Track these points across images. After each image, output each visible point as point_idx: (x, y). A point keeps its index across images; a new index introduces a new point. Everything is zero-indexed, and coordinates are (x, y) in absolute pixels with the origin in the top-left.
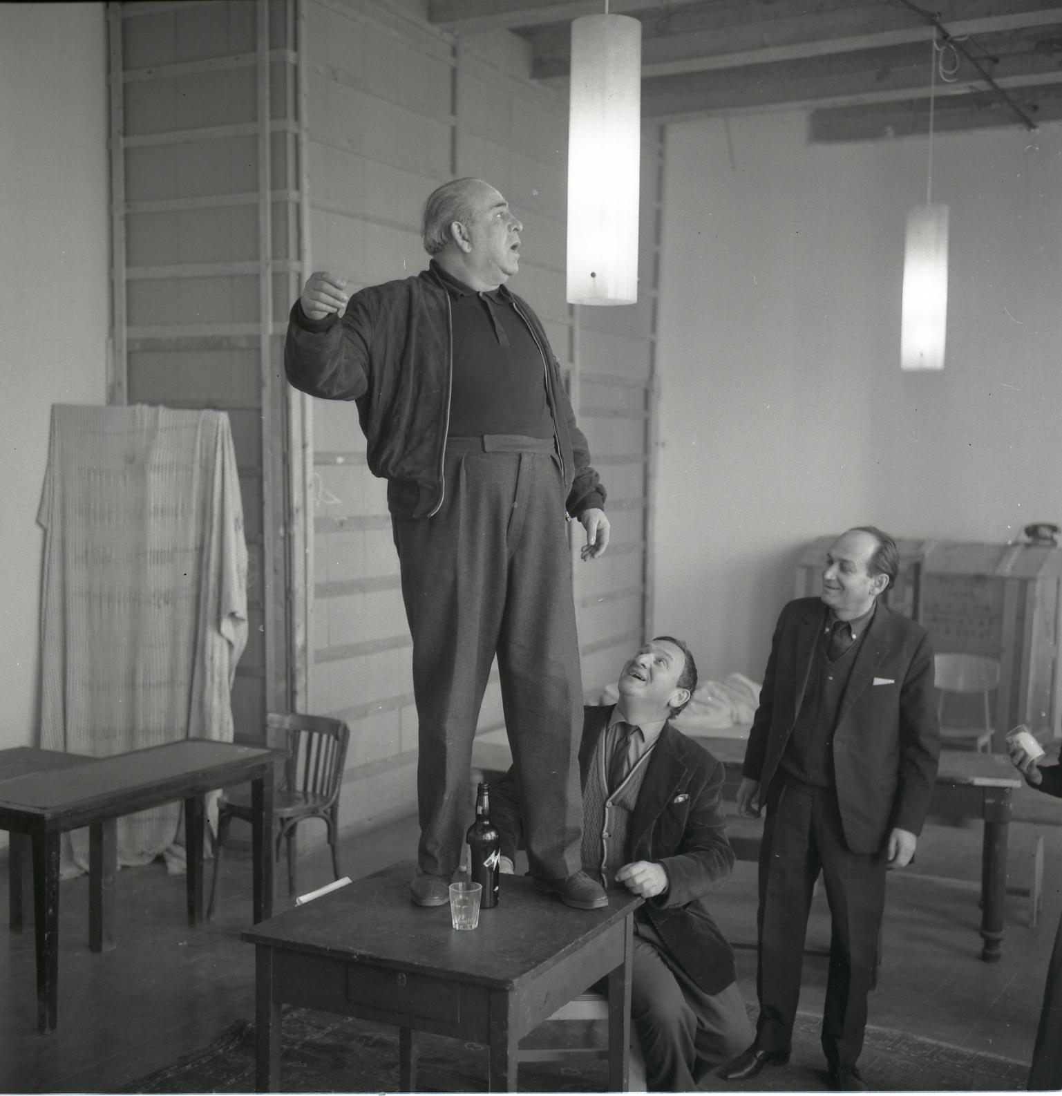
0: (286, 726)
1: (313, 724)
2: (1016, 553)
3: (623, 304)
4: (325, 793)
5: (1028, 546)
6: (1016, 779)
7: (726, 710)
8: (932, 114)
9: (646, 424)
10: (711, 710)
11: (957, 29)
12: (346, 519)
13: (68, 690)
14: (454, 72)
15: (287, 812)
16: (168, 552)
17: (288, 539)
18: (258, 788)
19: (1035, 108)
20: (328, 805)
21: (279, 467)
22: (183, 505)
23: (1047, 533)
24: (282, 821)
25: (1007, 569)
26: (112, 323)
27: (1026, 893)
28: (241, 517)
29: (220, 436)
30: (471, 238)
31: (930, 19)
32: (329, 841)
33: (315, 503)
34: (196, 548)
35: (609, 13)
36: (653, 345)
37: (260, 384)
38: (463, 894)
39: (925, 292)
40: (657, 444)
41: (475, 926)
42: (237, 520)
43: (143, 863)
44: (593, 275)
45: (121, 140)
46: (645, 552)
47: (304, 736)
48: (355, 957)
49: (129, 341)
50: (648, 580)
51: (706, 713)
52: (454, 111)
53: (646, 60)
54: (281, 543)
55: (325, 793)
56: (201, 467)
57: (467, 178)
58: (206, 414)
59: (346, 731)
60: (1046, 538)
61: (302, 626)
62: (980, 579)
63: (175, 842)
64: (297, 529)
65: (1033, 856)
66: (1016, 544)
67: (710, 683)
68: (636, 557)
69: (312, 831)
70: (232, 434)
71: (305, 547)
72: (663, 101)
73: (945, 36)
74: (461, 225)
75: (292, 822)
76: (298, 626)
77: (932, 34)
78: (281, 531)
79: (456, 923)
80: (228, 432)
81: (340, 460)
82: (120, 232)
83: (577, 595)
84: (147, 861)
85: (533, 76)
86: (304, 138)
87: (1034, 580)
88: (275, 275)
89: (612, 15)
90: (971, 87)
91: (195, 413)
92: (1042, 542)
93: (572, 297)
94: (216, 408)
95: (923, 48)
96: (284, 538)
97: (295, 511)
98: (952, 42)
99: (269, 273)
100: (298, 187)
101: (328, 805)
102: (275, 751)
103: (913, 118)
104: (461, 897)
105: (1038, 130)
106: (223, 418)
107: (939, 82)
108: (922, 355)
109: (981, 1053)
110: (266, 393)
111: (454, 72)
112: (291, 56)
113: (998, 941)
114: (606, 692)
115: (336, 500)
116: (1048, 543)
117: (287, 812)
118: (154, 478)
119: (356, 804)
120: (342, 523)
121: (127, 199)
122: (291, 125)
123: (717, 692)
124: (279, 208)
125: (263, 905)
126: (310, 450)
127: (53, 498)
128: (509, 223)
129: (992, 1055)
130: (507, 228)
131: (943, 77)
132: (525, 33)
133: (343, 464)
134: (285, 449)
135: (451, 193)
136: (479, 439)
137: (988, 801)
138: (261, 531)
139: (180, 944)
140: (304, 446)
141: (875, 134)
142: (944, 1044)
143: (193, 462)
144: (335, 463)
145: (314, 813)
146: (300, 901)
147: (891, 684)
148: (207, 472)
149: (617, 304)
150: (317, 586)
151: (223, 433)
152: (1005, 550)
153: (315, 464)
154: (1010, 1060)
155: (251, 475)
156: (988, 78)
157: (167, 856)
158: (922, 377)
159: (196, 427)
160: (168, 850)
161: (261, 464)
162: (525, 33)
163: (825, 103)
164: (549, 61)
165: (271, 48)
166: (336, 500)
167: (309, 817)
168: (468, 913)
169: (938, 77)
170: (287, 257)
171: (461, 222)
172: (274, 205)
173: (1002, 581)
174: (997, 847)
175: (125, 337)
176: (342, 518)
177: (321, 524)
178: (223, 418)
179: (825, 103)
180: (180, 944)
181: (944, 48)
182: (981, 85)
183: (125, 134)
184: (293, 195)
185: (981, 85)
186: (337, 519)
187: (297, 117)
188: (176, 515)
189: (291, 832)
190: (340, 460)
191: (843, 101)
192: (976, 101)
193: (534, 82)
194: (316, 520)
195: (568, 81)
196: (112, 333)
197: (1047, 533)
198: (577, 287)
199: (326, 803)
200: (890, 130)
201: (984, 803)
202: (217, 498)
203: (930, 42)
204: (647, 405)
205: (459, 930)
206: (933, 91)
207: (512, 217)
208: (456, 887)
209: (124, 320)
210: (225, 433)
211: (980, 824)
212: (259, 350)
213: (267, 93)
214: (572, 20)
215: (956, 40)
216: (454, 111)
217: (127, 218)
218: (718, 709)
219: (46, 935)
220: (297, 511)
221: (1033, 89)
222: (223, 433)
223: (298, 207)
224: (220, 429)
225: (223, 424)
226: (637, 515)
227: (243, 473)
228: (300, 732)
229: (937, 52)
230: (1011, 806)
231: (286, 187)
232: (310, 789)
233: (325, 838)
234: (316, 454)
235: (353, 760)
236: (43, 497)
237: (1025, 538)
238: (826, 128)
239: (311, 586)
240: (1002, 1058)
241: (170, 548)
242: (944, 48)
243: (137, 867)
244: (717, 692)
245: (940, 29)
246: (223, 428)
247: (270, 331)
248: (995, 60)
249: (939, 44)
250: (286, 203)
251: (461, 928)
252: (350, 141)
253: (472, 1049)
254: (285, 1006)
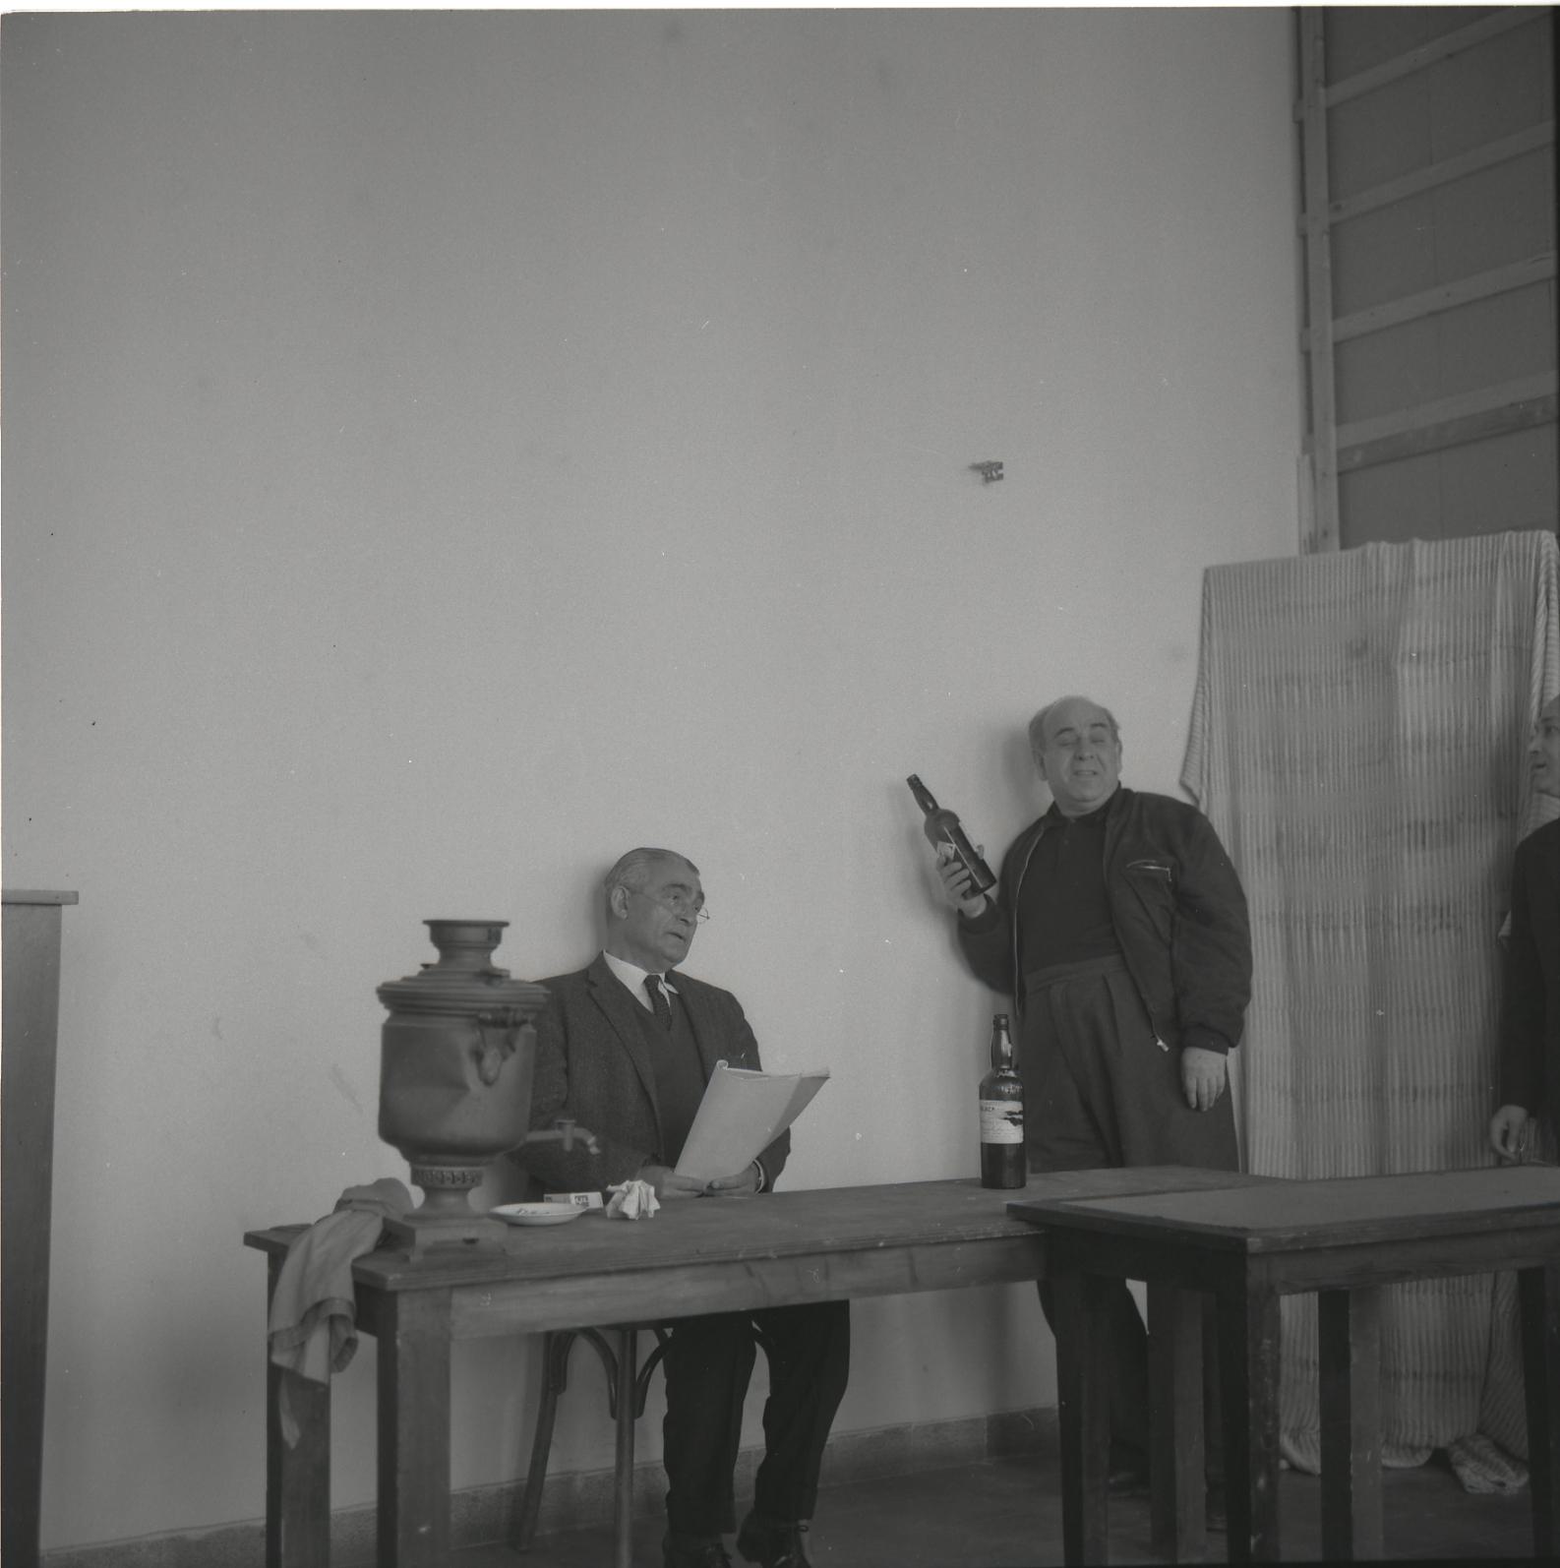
13: (1252, 1103)
26: (1309, 427)
29: (1542, 578)
43: (1416, 1464)
45: (1322, 90)
49: (1340, 453)
82: (1321, 262)
84: (1422, 1458)
93: (1224, 1560)
118: (1405, 673)
121: (1332, 196)
127: (1210, 741)
143: (1488, 637)
147: (1145, 1333)
157: (1457, 1454)
159: (1494, 568)
175: (1333, 448)
183: (1328, 82)
196: (1307, 447)
209: (1332, 416)
211: (781, 1185)
217: (1334, 230)
219: (1253, 1541)
225: (1548, 553)
236: (1191, 738)
243: (1396, 1469)
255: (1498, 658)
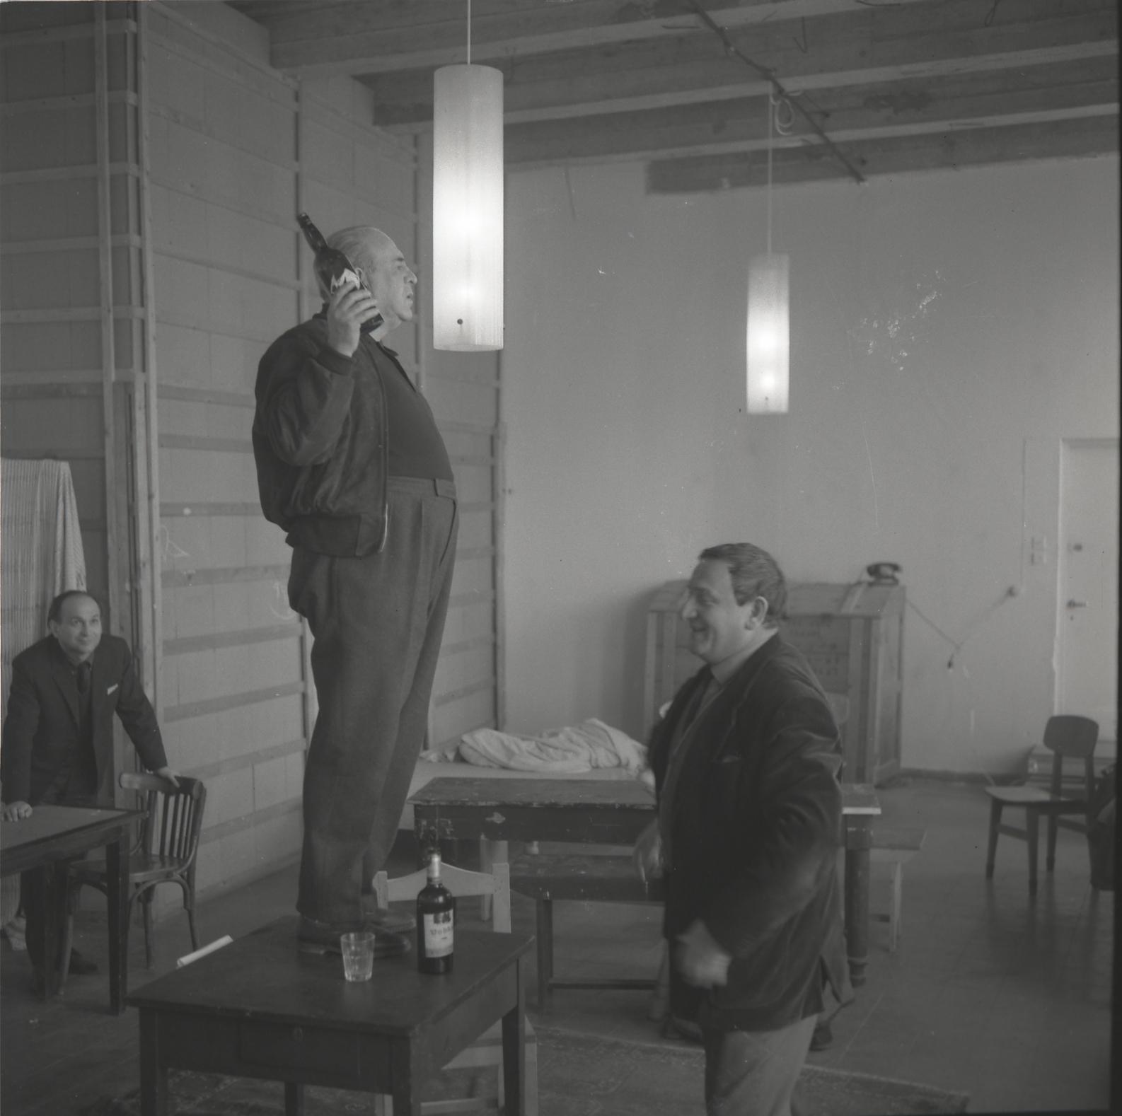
0: (136, 786)
1: (168, 787)
2: (859, 592)
3: (487, 350)
4: (182, 856)
5: (871, 584)
6: (876, 807)
7: (585, 754)
8: (770, 165)
9: (493, 469)
10: (570, 755)
11: (793, 85)
12: (194, 572)
14: (297, 117)
15: (137, 877)
16: (8, 610)
17: (135, 594)
18: (114, 852)
19: (863, 162)
20: (184, 868)
21: (124, 519)
22: (23, 561)
23: (888, 571)
24: (137, 885)
25: (851, 607)
27: (886, 919)
28: (83, 574)
29: (61, 487)
30: (371, 285)
31: (767, 75)
32: (185, 906)
33: (162, 557)
34: (37, 606)
35: (471, 63)
36: (498, 392)
37: (103, 432)
38: (356, 946)
39: (768, 341)
40: (504, 490)
41: (369, 975)
42: (79, 575)
44: (460, 322)
46: (495, 602)
47: (161, 797)
48: (248, 1014)
50: (499, 630)
51: (565, 758)
52: (297, 158)
53: (507, 109)
54: (127, 599)
55: (182, 856)
56: (41, 520)
57: (353, 228)
58: (45, 463)
59: (202, 790)
60: (887, 577)
61: (151, 684)
62: (826, 618)
63: (18, 914)
64: (144, 584)
65: (892, 882)
66: (859, 583)
67: (568, 729)
68: (486, 608)
69: (168, 896)
70: (74, 484)
71: (153, 602)
72: (525, 149)
73: (780, 92)
74: (362, 271)
75: (148, 885)
76: (147, 684)
77: (767, 88)
78: (127, 587)
79: (348, 976)
80: (69, 482)
81: (187, 511)
83: (443, 644)
85: (375, 123)
86: (146, 181)
87: (878, 617)
88: (116, 321)
89: (473, 66)
90: (804, 140)
91: (35, 462)
92: (884, 581)
94: (55, 458)
95: (758, 103)
96: (131, 594)
97: (141, 565)
98: (787, 96)
99: (111, 317)
100: (140, 231)
101: (184, 868)
102: (130, 813)
103: (750, 170)
104: (353, 948)
105: (867, 184)
106: (65, 467)
107: (776, 135)
108: (767, 399)
109: (856, 1074)
110: (109, 442)
111: (297, 117)
112: (131, 98)
113: (862, 966)
114: (462, 742)
115: (184, 554)
116: (890, 581)
117: (137, 877)
119: (215, 864)
120: (190, 577)
122: (132, 168)
123: (575, 737)
124: (120, 252)
125: (120, 977)
126: (156, 501)
128: (404, 275)
129: (866, 1076)
130: (403, 278)
131: (781, 133)
132: (367, 80)
133: (190, 515)
134: (131, 499)
135: (351, 239)
136: (431, 483)
137: (850, 829)
138: (106, 587)
139: (31, 1021)
140: (150, 497)
141: (711, 185)
142: (820, 1069)
144: (182, 515)
145: (168, 877)
146: (180, 962)
148: (49, 525)
149: (483, 349)
150: (165, 643)
151: (64, 484)
152: (849, 589)
153: (161, 515)
154: (883, 1079)
155: (94, 529)
156: (820, 132)
157: (10, 931)
158: (768, 420)
160: (10, 925)
161: (104, 517)
162: (367, 80)
163: (663, 154)
164: (405, 112)
165: (110, 89)
166: (184, 554)
167: (163, 881)
168: (362, 964)
169: (774, 129)
170: (130, 303)
171: (363, 269)
172: (115, 250)
173: (848, 618)
174: (860, 873)
176: (190, 572)
177: (166, 577)
178: (65, 467)
179: (663, 154)
180: (31, 1021)
181: (779, 102)
182: (814, 139)
184: (135, 239)
185: (814, 139)
186: (185, 573)
187: (138, 160)
188: (16, 571)
189: (148, 894)
190: (187, 511)
191: (680, 152)
192: (809, 153)
193: (378, 129)
194: (163, 575)
195: (430, 132)
197: (888, 571)
198: (444, 329)
199: (181, 866)
200: (726, 182)
201: (847, 831)
202: (59, 553)
203: (766, 97)
204: (493, 452)
205: (353, 983)
206: (770, 143)
207: (408, 269)
208: (348, 938)
210: (67, 484)
212: (101, 398)
213: (106, 135)
214: (433, 68)
215: (791, 95)
216: (297, 158)
218: (576, 754)
220: (144, 565)
221: (861, 143)
222: (64, 484)
223: (141, 252)
224: (62, 478)
226: (487, 563)
227: (85, 526)
228: (156, 793)
229: (774, 106)
230: (872, 833)
231: (127, 231)
232: (167, 853)
233: (181, 903)
234: (162, 506)
235: (210, 817)
237: (867, 578)
238: (665, 179)
239: (159, 642)
240: (875, 1077)
241: (10, 606)
242: (779, 102)
244: (575, 737)
245: (776, 85)
246: (64, 479)
247: (113, 377)
248: (826, 115)
249: (776, 99)
250: (128, 249)
251: (354, 979)
252: (192, 186)
253: (353, 1109)
254: (170, 1070)
255: (37, 524)
